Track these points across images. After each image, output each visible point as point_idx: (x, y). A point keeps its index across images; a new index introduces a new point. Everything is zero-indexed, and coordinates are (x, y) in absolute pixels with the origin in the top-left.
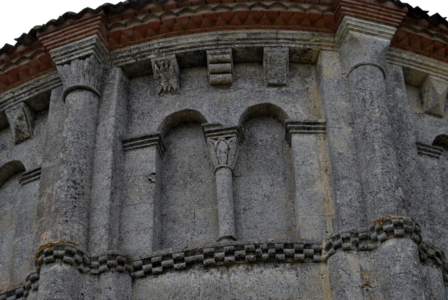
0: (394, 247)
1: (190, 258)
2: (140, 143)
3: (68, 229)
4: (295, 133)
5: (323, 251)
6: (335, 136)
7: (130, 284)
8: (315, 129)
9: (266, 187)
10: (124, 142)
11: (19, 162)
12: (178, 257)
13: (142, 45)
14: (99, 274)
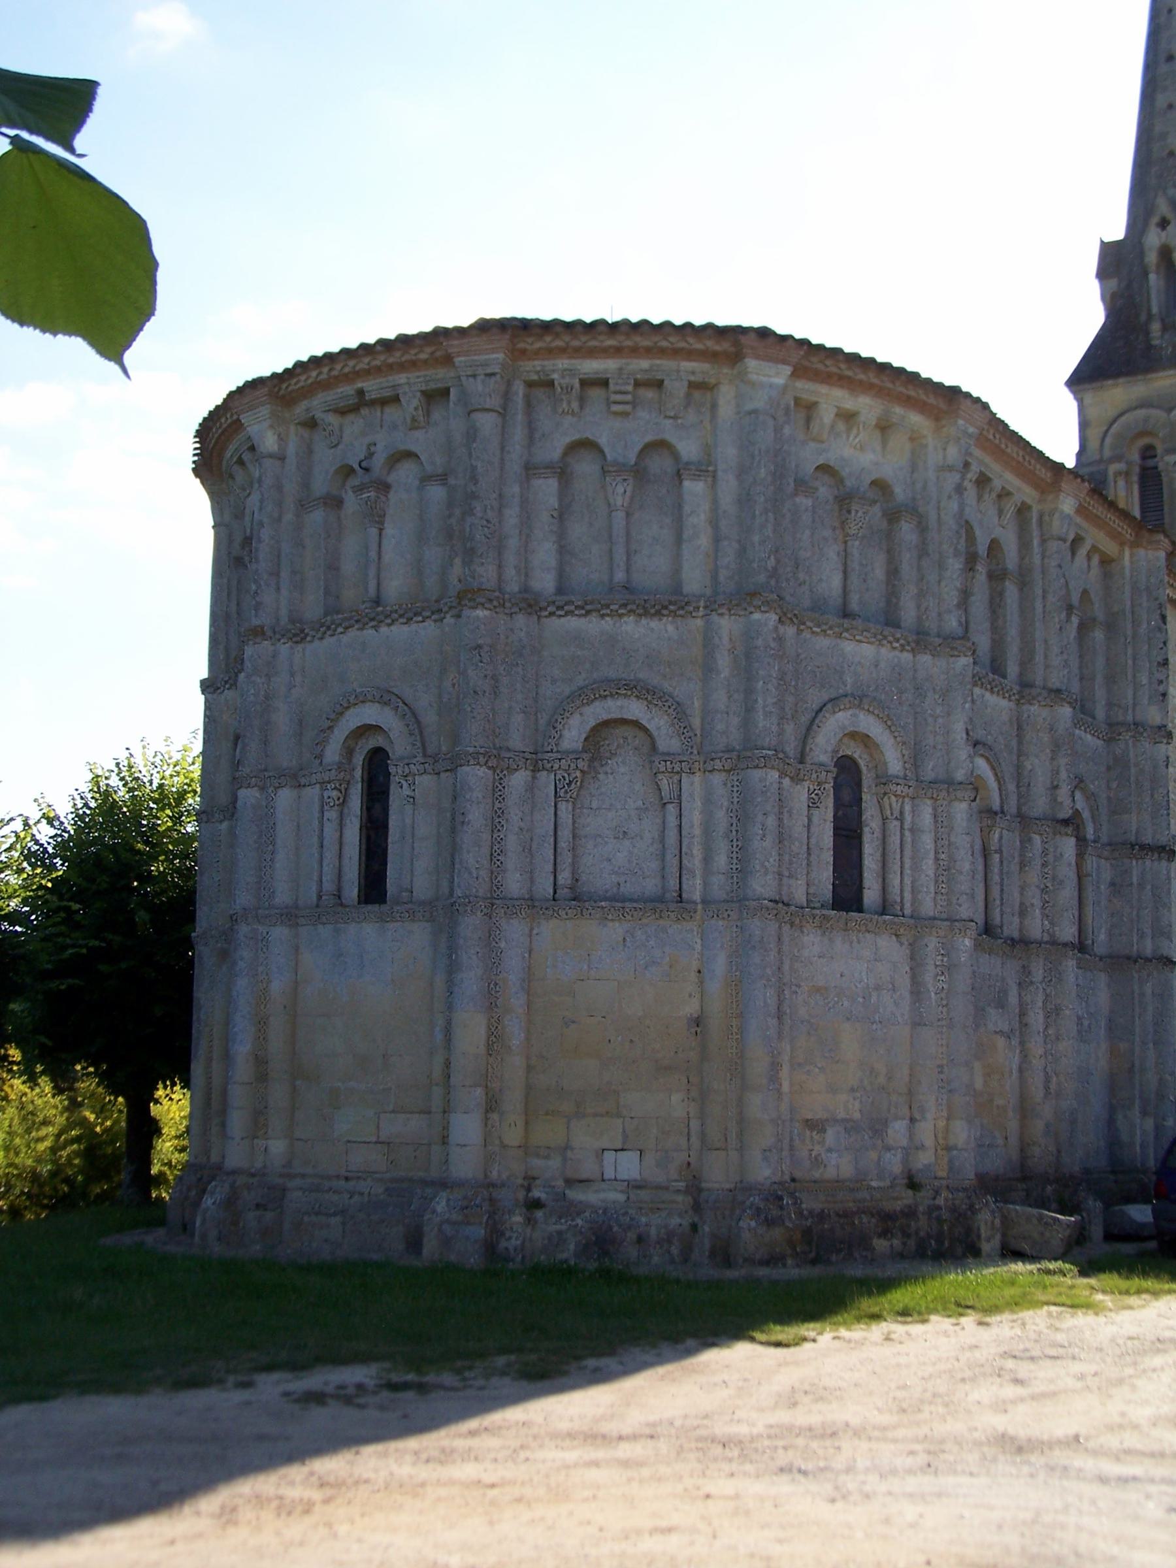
1: (588, 607)
5: (701, 609)
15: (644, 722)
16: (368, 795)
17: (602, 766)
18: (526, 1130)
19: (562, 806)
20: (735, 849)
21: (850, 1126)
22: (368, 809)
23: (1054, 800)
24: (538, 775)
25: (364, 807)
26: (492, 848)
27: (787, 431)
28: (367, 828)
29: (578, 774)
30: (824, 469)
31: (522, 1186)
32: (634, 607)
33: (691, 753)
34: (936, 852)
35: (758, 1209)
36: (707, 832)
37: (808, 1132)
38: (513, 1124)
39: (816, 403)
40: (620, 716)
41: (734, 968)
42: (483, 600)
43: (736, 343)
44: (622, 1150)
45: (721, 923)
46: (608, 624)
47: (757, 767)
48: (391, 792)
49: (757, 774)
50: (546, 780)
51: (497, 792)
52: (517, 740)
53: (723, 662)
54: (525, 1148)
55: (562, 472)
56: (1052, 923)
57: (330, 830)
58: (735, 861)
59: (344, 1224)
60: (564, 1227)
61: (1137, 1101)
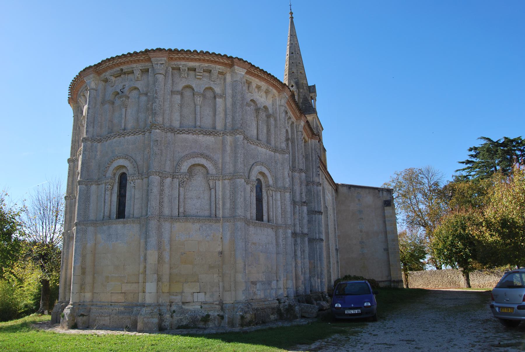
1: (189, 132)
13: (178, 62)
15: (205, 165)
16: (120, 187)
18: (170, 288)
19: (181, 189)
20: (232, 202)
21: (263, 283)
22: (120, 191)
23: (301, 196)
25: (118, 190)
27: (244, 88)
28: (119, 197)
29: (186, 179)
30: (252, 101)
31: (169, 305)
32: (203, 132)
34: (281, 206)
35: (242, 309)
36: (223, 198)
37: (252, 285)
39: (251, 82)
42: (158, 127)
43: (232, 62)
44: (199, 292)
45: (228, 223)
46: (195, 136)
48: (127, 186)
49: (238, 180)
50: (176, 181)
51: (162, 184)
52: (168, 168)
53: (228, 148)
54: (169, 293)
55: (182, 94)
56: (302, 229)
57: (108, 197)
58: (232, 205)
59: (110, 319)
60: (182, 317)
61: (316, 275)
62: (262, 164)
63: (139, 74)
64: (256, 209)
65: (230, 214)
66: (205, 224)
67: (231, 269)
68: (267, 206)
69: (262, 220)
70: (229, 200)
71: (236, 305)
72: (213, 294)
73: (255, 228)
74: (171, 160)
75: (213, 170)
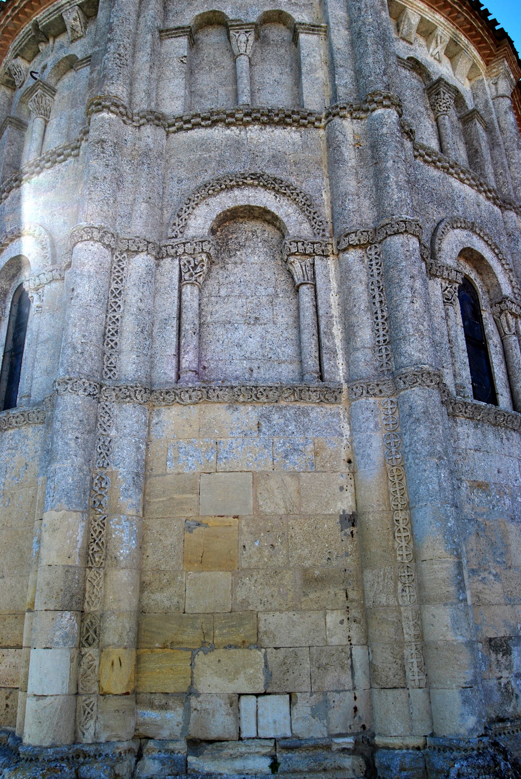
0: (382, 114)
1: (215, 118)
2: (174, 33)
3: (114, 89)
4: (302, 33)
5: (323, 120)
6: (335, 36)
7: (165, 137)
8: (318, 31)
9: (276, 74)
10: (161, 32)
11: (74, 55)
12: (205, 116)
14: (139, 127)
15: (273, 209)
17: (231, 257)
19: (187, 289)
20: (380, 321)
24: (162, 263)
26: (106, 328)
29: (204, 257)
31: (130, 750)
33: (323, 236)
37: (493, 656)
38: (117, 662)
40: (247, 203)
41: (393, 450)
42: (108, 104)
44: (265, 694)
45: (372, 400)
46: (234, 132)
47: (396, 233)
49: (398, 240)
58: (381, 333)
62: (472, 228)
63: (75, 19)
64: (470, 365)
65: (377, 364)
66: (281, 409)
67: (400, 586)
68: (503, 366)
69: (493, 399)
70: (369, 315)
71: (439, 762)
72: (326, 701)
73: (476, 427)
74: (152, 201)
75: (301, 224)
